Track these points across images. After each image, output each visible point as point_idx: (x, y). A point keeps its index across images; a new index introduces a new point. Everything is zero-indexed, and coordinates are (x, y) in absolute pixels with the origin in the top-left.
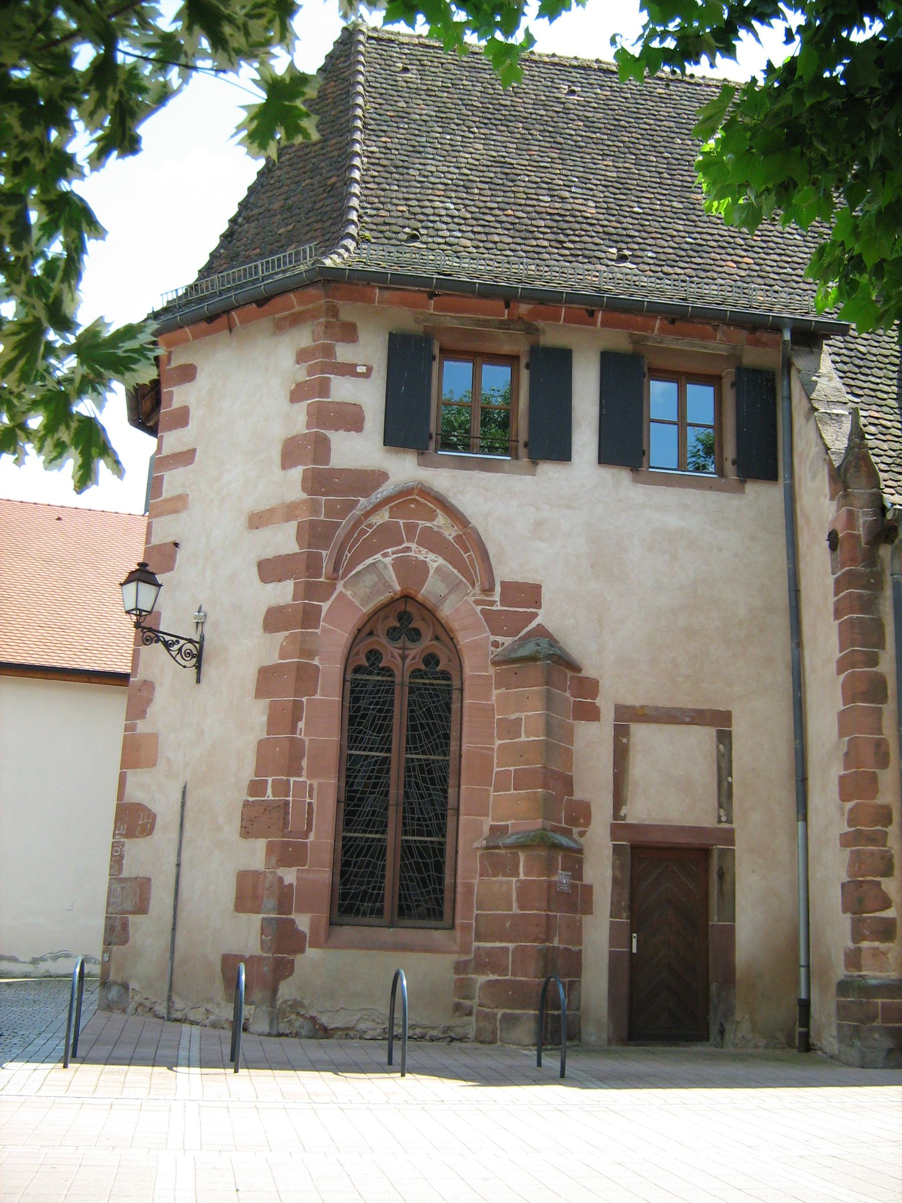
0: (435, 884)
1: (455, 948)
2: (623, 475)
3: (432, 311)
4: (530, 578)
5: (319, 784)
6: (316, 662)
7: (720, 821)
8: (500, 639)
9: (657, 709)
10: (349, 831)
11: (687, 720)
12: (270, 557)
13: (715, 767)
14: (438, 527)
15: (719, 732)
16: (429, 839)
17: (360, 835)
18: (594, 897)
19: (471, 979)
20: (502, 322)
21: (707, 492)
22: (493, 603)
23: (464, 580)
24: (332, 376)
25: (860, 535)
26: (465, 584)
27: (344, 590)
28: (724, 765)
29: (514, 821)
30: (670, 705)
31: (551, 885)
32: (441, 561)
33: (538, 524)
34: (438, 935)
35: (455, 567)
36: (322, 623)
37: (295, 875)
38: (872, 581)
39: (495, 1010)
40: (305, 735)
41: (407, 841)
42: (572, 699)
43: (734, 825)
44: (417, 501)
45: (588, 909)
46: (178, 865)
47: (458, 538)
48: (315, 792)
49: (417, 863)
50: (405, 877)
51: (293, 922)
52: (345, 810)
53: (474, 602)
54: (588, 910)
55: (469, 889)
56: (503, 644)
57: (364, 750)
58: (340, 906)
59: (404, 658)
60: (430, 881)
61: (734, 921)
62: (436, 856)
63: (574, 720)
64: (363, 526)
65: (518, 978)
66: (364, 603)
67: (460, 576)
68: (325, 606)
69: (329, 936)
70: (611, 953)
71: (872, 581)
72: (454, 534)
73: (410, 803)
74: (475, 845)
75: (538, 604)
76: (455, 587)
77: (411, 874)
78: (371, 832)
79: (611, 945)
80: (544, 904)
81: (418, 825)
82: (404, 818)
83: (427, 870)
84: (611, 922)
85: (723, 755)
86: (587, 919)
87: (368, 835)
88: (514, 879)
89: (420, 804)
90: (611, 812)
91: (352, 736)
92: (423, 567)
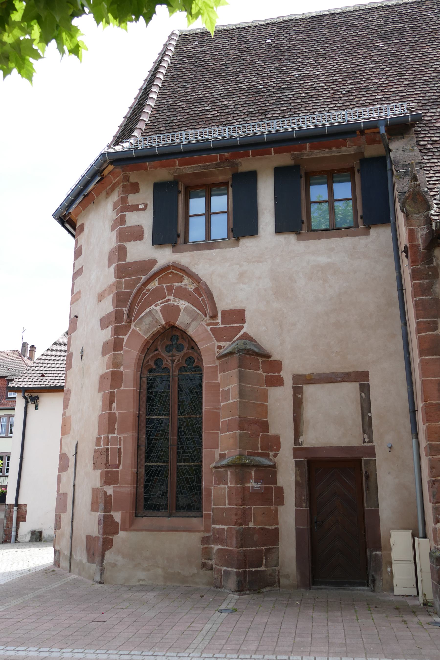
0: (197, 490)
1: (203, 528)
2: (291, 238)
3: (178, 167)
4: (238, 306)
5: (124, 437)
6: (121, 369)
7: (364, 442)
8: (222, 344)
9: (319, 375)
10: (149, 462)
11: (339, 379)
12: (104, 316)
13: (360, 406)
14: (185, 285)
15: (361, 385)
16: (193, 464)
17: (154, 464)
18: (285, 495)
19: (211, 547)
20: (217, 164)
21: (345, 239)
22: (217, 324)
23: (200, 313)
24: (126, 213)
25: (419, 245)
26: (201, 315)
27: (135, 328)
28: (365, 405)
29: (228, 451)
30: (327, 372)
31: (244, 489)
32: (187, 304)
33: (242, 275)
34: (195, 520)
35: (195, 306)
36: (124, 348)
37: (112, 489)
38: (430, 273)
39: (221, 567)
40: (116, 411)
41: (181, 466)
42: (265, 374)
43: (374, 444)
44: (173, 273)
45: (281, 501)
46: (74, 486)
47: (196, 290)
48: (122, 442)
49: (186, 478)
50: (180, 486)
51: (112, 516)
52: (146, 450)
53: (206, 325)
54: (281, 502)
55: (209, 492)
56: (224, 347)
57: (156, 416)
58: (145, 505)
59: (173, 361)
60: (194, 489)
61: (378, 507)
62: (197, 473)
63: (267, 386)
64: (144, 291)
65: (229, 548)
66: (146, 333)
67: (198, 311)
68: (125, 338)
69: (132, 523)
70: (297, 529)
71: (430, 273)
72: (193, 288)
73: (182, 444)
74: (212, 466)
75: (243, 321)
76: (195, 318)
77: (183, 485)
78: (160, 462)
79: (296, 525)
80: (240, 502)
81: (186, 456)
82: (178, 452)
83: (192, 482)
84: (296, 509)
85: (364, 400)
86: (281, 509)
87: (159, 464)
88: (226, 486)
89: (187, 444)
90: (293, 441)
91: (149, 408)
92: (177, 309)
